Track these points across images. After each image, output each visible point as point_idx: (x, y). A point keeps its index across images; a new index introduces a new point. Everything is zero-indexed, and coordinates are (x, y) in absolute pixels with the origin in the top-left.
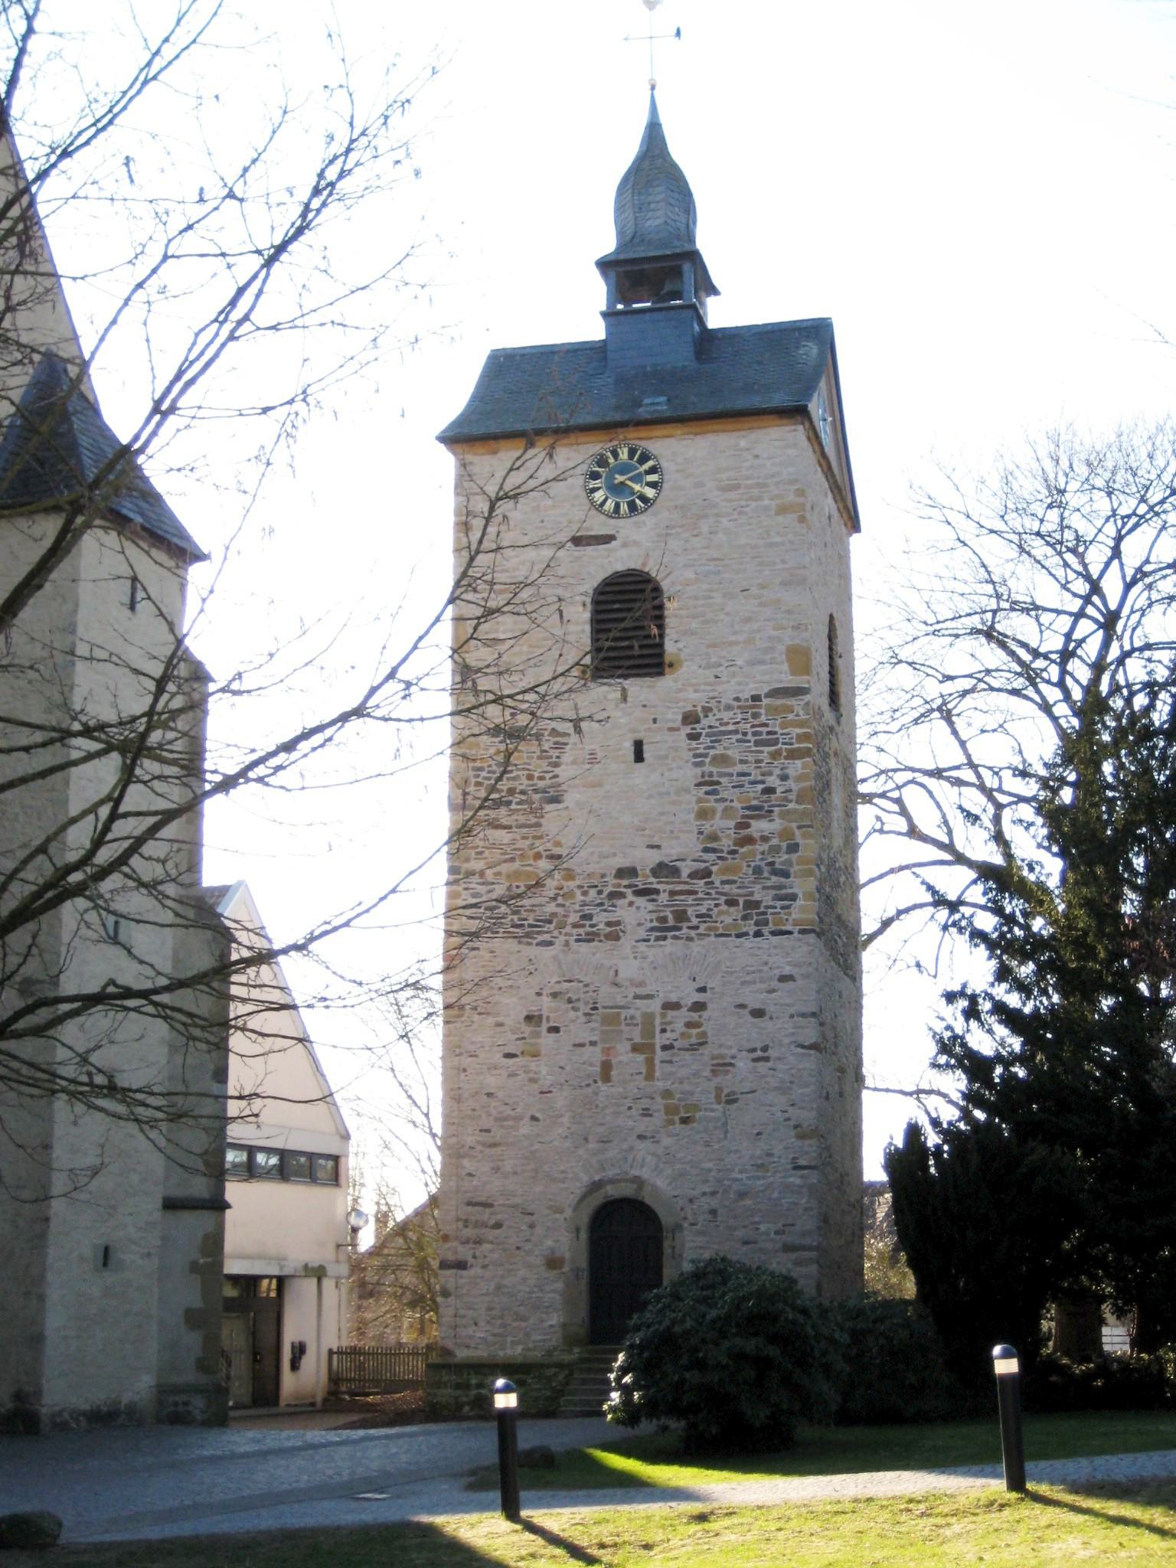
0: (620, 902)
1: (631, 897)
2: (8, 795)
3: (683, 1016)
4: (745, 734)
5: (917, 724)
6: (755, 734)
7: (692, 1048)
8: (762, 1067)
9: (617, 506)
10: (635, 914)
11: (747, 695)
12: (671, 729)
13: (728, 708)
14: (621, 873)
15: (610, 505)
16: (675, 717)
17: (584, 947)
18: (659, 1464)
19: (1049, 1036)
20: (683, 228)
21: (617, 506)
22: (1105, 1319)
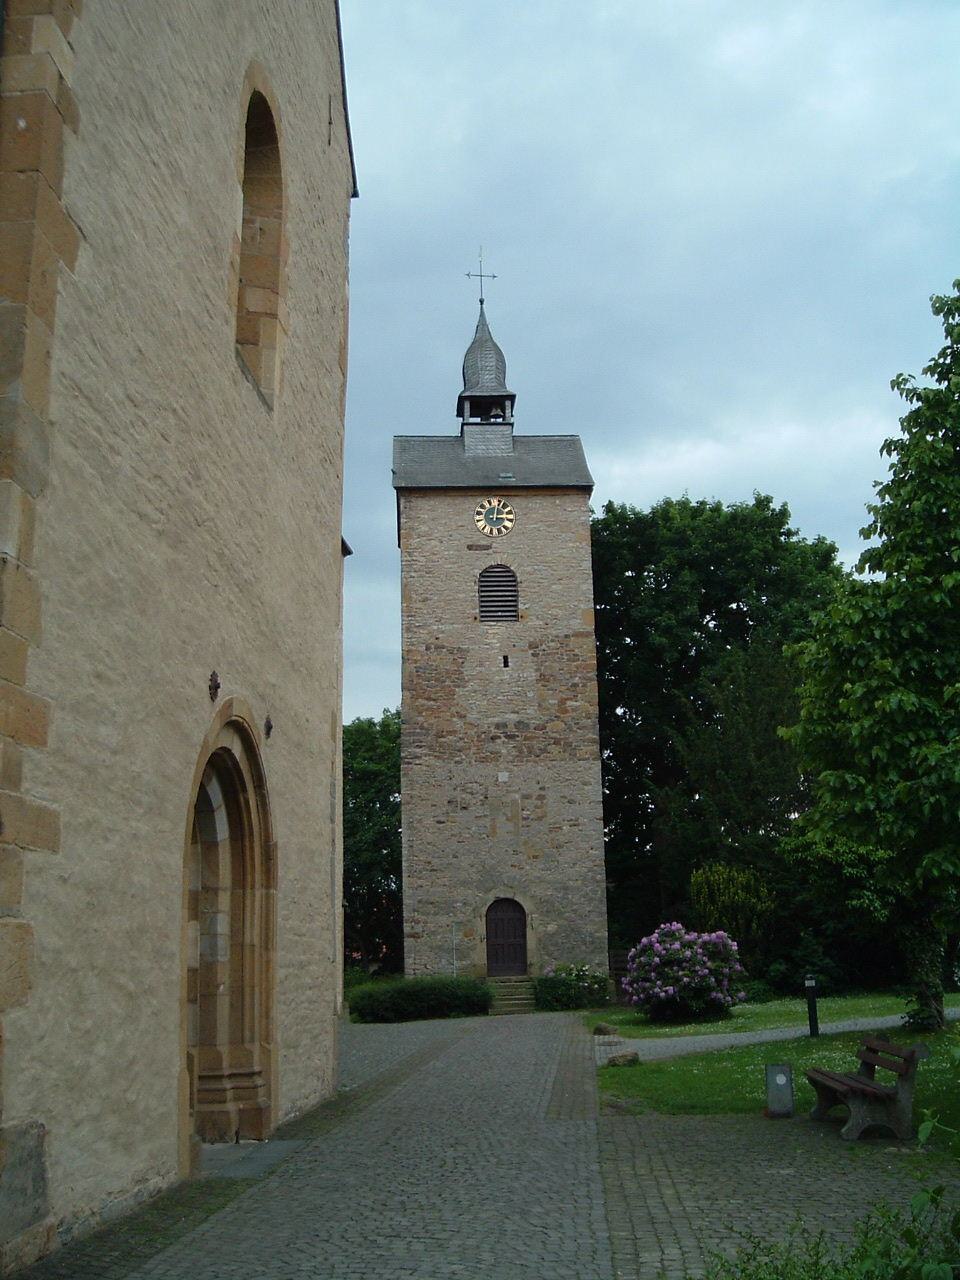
0: (498, 741)
1: (503, 739)
2: (333, 3)
3: (534, 801)
4: (562, 655)
5: (219, 765)
6: (567, 655)
7: (540, 819)
8: (575, 829)
9: (491, 530)
10: (504, 748)
11: (562, 635)
12: (523, 651)
13: (552, 641)
14: (498, 726)
15: (495, 531)
16: (524, 644)
17: (481, 766)
18: (434, 1019)
19: (794, 816)
20: (402, 501)
21: (491, 530)
22: (54, 811)
